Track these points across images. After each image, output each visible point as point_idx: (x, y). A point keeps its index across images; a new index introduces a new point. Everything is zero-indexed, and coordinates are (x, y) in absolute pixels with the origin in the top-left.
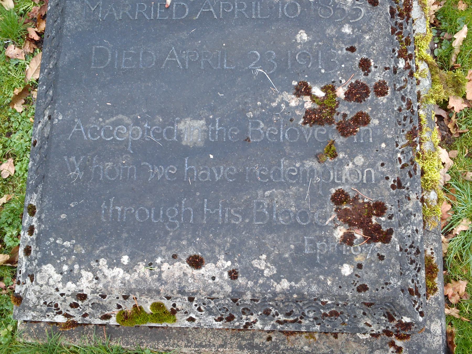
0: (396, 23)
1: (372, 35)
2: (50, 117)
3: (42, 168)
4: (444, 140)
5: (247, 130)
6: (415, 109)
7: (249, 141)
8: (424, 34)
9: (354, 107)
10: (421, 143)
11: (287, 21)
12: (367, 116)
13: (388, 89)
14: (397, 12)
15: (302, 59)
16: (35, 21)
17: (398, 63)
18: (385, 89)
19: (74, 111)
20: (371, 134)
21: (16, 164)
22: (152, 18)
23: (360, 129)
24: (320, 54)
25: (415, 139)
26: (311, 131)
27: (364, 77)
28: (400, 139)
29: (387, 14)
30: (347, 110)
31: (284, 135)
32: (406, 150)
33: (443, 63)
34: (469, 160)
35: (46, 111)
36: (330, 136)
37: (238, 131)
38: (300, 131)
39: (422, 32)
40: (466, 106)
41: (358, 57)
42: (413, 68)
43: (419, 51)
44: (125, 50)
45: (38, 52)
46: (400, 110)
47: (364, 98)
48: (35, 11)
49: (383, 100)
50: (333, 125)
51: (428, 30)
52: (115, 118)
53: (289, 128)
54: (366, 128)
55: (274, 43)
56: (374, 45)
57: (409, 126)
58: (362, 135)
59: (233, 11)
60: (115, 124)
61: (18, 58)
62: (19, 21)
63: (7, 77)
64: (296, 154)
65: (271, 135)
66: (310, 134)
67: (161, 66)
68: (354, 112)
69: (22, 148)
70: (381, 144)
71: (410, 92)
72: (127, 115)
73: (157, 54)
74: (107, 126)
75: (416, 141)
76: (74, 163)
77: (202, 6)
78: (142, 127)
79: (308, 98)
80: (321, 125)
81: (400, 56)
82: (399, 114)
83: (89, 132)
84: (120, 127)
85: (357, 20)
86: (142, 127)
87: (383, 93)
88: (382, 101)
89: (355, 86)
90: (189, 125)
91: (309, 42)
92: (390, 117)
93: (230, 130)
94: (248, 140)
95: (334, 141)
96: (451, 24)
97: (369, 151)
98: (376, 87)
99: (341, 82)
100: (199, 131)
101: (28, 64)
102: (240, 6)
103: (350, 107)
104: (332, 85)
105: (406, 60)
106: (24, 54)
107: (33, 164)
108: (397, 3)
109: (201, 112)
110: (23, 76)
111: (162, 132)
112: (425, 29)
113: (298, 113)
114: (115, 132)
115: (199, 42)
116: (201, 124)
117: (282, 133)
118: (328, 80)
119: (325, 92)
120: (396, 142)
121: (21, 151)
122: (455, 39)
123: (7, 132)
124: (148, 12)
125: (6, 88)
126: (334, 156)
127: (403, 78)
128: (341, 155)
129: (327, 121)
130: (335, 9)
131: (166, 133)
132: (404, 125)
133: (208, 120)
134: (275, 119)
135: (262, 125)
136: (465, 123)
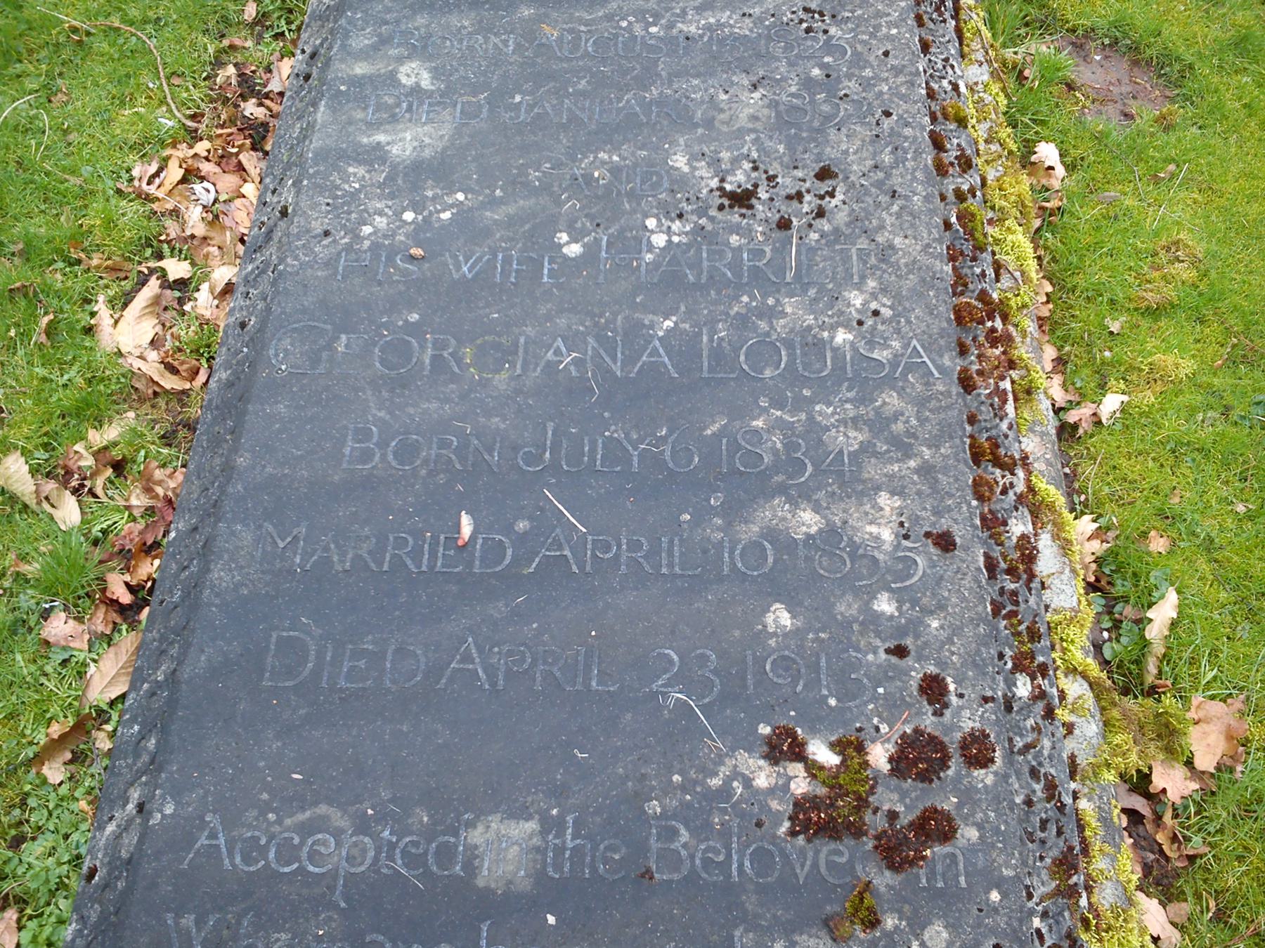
0: (1002, 591)
1: (945, 618)
2: (141, 807)
3: (103, 942)
4: (1150, 873)
5: (643, 849)
6: (1068, 800)
7: (651, 878)
8: (1072, 609)
9: (913, 795)
10: (1089, 889)
11: (744, 581)
12: (948, 818)
13: (994, 751)
14: (1003, 565)
15: (781, 671)
16: (127, 558)
17: (1015, 685)
18: (987, 750)
19: (207, 792)
20: (961, 866)
21: (24, 927)
22: (424, 568)
23: (933, 852)
24: (823, 660)
25: (1075, 879)
26: (810, 854)
27: (933, 718)
28: (1035, 878)
29: (979, 569)
30: (897, 801)
31: (741, 864)
32: (1053, 910)
33: (1125, 678)
34: (1222, 930)
35: (132, 790)
36: (859, 868)
37: (624, 850)
38: (782, 852)
39: (1067, 606)
40: (1195, 786)
41: (916, 671)
42: (1052, 698)
43: (1064, 650)
44: (351, 642)
45: (124, 633)
46: (1029, 802)
47: (937, 773)
48: (131, 533)
49: (984, 777)
50: (865, 839)
51: (1083, 599)
52: (308, 814)
53: (754, 846)
54: (947, 849)
55: (713, 631)
56: (953, 643)
57: (1056, 845)
58: (939, 868)
59: (617, 556)
60: (306, 829)
61: (72, 645)
62: (89, 556)
63: (37, 691)
64: (774, 916)
65: (707, 863)
66: (808, 863)
67: (438, 683)
68: (916, 807)
69: (47, 881)
70: (988, 892)
71: (1050, 757)
72: (342, 807)
73: (430, 655)
74: (286, 835)
75: (1076, 884)
76: (190, 932)
77: (544, 543)
78: (376, 837)
79: (797, 769)
80: (836, 839)
81: (1018, 667)
82: (1027, 813)
83: (237, 850)
84: (320, 836)
85: (908, 583)
86: (376, 837)
87: (983, 761)
88: (982, 781)
89: (913, 742)
90: (498, 833)
91: (797, 633)
92: (1006, 822)
93: (602, 847)
94: (648, 874)
95: (870, 882)
96: (1137, 586)
97: (960, 911)
98: (964, 746)
99: (877, 729)
100: (522, 849)
101: (95, 661)
102: (634, 546)
103: (903, 795)
104: (857, 738)
105: (1033, 678)
106: (87, 637)
107: (80, 931)
108: (1001, 544)
109: (530, 799)
110: (76, 690)
111: (426, 853)
112: (1075, 598)
113: (775, 805)
114: (306, 849)
115: (535, 626)
116: (529, 831)
117: (735, 857)
118: (845, 724)
119: (838, 754)
120: (1027, 887)
121: (44, 890)
122: (1151, 620)
123: (13, 837)
124: (416, 554)
125: (28, 721)
126: (872, 923)
127: (1030, 722)
128: (890, 922)
129: (848, 828)
130: (853, 556)
131: (438, 853)
132: (1043, 842)
133: (545, 820)
134: (717, 820)
135: (684, 835)
136: (1200, 830)
